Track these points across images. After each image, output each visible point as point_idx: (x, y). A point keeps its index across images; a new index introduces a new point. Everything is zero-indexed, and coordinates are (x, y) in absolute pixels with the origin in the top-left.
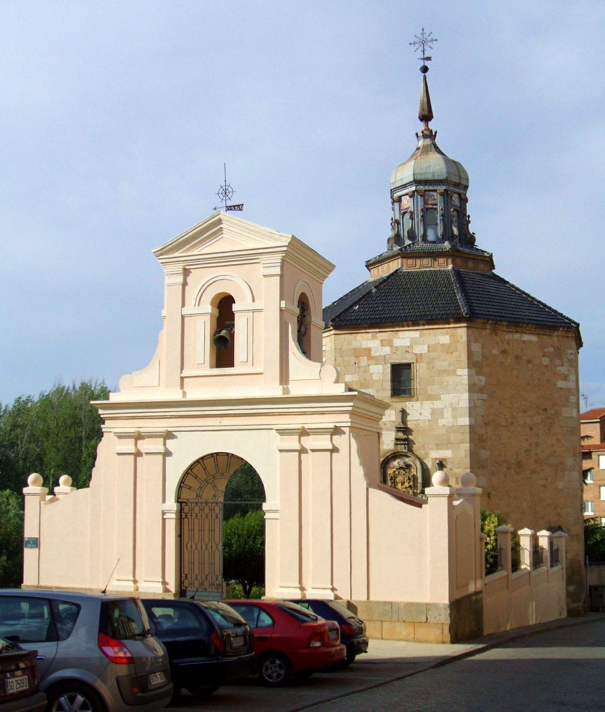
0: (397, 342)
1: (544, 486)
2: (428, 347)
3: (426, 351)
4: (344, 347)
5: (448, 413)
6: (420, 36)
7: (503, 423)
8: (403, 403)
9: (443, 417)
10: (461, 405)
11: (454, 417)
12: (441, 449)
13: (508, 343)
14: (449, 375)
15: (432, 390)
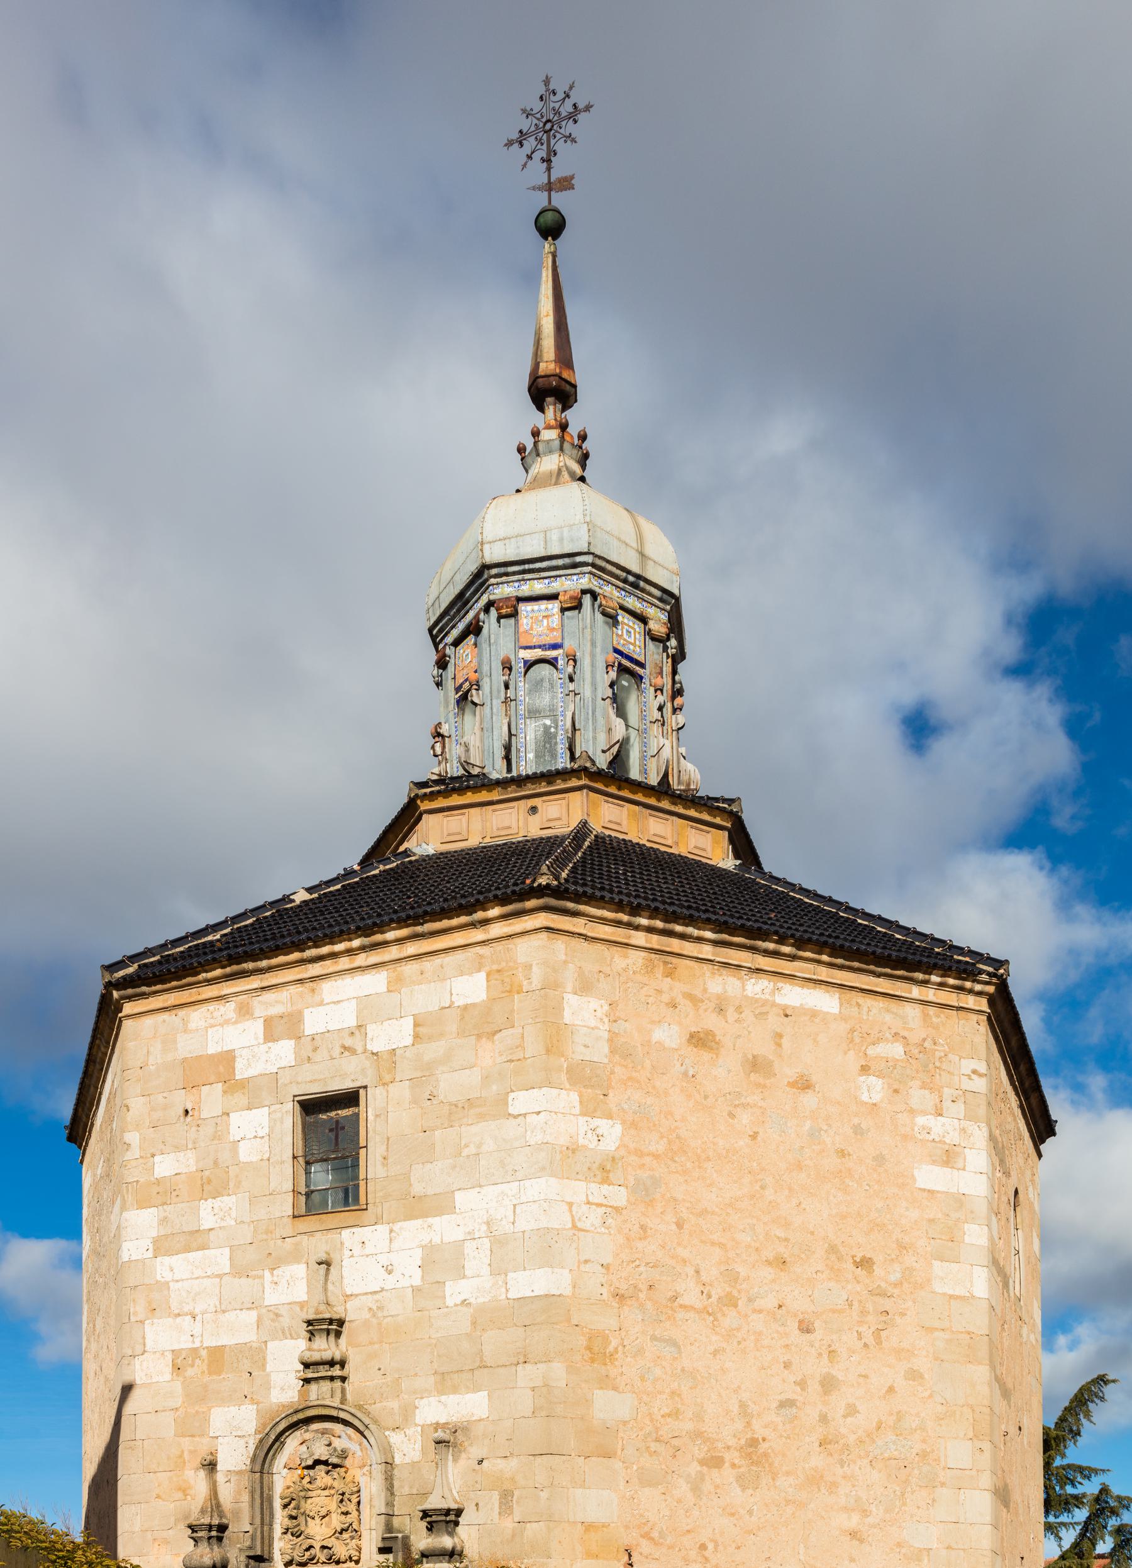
0: (315, 1021)
1: (853, 1534)
2: (416, 1025)
3: (409, 1041)
4: (151, 1060)
5: (477, 1260)
6: (537, 106)
7: (691, 1297)
8: (332, 1235)
9: (460, 1273)
10: (522, 1225)
11: (499, 1270)
12: (455, 1390)
13: (721, 1010)
14: (482, 1117)
15: (427, 1178)
